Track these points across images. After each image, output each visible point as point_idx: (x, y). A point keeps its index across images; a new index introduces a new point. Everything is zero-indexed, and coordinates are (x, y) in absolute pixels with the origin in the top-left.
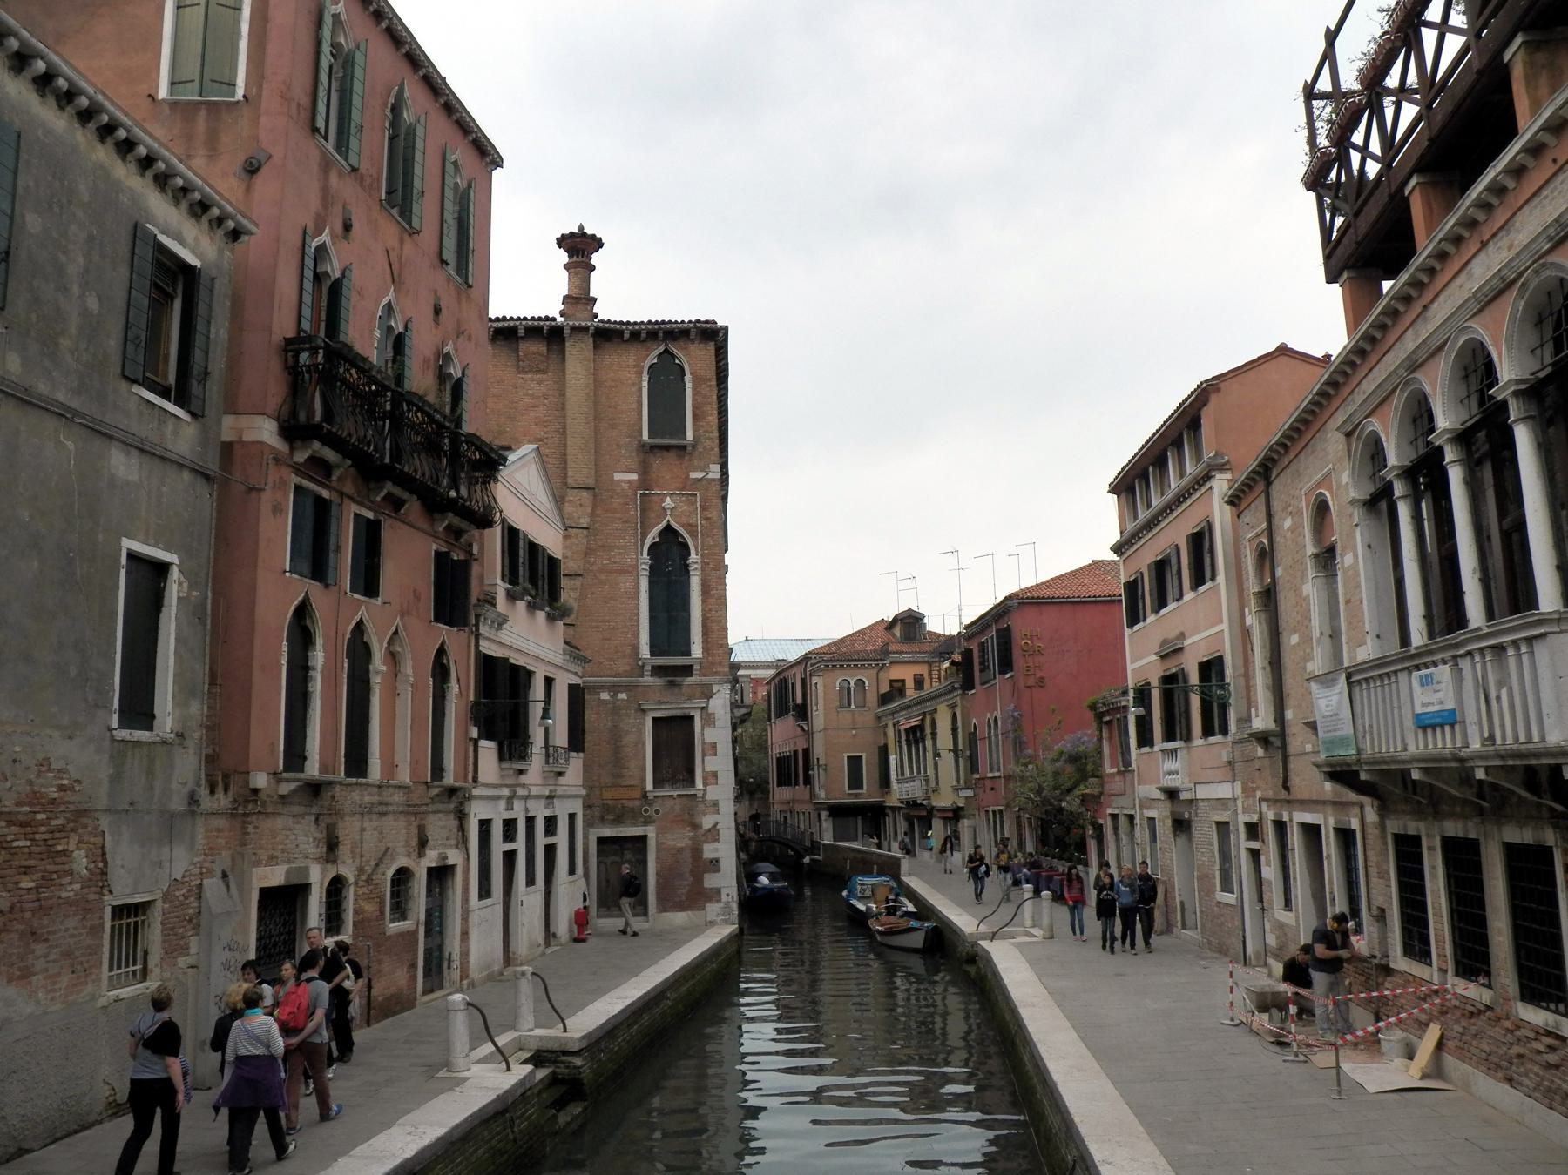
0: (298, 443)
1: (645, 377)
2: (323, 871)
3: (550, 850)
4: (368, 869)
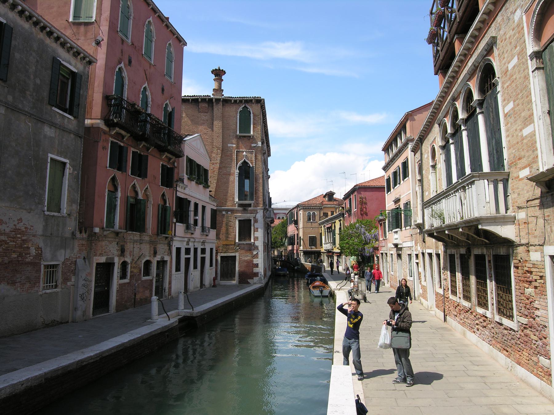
0: (112, 128)
1: (238, 115)
2: (119, 259)
3: (203, 259)
4: (136, 260)
